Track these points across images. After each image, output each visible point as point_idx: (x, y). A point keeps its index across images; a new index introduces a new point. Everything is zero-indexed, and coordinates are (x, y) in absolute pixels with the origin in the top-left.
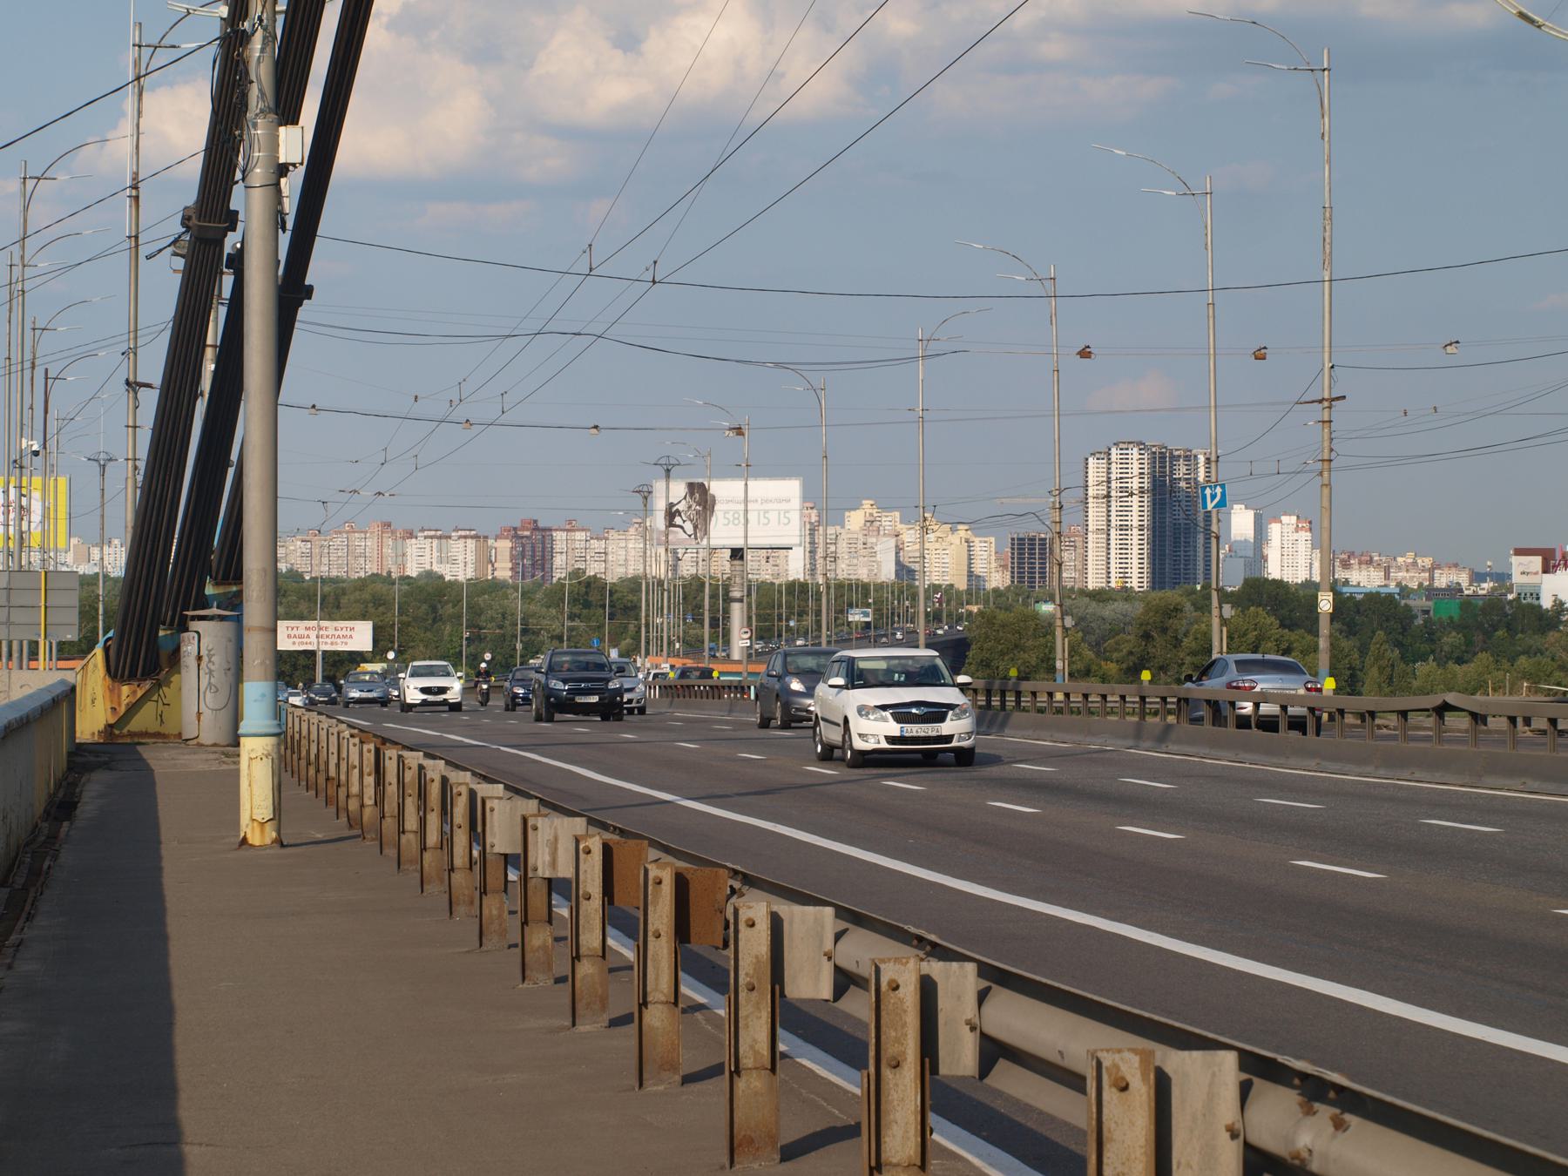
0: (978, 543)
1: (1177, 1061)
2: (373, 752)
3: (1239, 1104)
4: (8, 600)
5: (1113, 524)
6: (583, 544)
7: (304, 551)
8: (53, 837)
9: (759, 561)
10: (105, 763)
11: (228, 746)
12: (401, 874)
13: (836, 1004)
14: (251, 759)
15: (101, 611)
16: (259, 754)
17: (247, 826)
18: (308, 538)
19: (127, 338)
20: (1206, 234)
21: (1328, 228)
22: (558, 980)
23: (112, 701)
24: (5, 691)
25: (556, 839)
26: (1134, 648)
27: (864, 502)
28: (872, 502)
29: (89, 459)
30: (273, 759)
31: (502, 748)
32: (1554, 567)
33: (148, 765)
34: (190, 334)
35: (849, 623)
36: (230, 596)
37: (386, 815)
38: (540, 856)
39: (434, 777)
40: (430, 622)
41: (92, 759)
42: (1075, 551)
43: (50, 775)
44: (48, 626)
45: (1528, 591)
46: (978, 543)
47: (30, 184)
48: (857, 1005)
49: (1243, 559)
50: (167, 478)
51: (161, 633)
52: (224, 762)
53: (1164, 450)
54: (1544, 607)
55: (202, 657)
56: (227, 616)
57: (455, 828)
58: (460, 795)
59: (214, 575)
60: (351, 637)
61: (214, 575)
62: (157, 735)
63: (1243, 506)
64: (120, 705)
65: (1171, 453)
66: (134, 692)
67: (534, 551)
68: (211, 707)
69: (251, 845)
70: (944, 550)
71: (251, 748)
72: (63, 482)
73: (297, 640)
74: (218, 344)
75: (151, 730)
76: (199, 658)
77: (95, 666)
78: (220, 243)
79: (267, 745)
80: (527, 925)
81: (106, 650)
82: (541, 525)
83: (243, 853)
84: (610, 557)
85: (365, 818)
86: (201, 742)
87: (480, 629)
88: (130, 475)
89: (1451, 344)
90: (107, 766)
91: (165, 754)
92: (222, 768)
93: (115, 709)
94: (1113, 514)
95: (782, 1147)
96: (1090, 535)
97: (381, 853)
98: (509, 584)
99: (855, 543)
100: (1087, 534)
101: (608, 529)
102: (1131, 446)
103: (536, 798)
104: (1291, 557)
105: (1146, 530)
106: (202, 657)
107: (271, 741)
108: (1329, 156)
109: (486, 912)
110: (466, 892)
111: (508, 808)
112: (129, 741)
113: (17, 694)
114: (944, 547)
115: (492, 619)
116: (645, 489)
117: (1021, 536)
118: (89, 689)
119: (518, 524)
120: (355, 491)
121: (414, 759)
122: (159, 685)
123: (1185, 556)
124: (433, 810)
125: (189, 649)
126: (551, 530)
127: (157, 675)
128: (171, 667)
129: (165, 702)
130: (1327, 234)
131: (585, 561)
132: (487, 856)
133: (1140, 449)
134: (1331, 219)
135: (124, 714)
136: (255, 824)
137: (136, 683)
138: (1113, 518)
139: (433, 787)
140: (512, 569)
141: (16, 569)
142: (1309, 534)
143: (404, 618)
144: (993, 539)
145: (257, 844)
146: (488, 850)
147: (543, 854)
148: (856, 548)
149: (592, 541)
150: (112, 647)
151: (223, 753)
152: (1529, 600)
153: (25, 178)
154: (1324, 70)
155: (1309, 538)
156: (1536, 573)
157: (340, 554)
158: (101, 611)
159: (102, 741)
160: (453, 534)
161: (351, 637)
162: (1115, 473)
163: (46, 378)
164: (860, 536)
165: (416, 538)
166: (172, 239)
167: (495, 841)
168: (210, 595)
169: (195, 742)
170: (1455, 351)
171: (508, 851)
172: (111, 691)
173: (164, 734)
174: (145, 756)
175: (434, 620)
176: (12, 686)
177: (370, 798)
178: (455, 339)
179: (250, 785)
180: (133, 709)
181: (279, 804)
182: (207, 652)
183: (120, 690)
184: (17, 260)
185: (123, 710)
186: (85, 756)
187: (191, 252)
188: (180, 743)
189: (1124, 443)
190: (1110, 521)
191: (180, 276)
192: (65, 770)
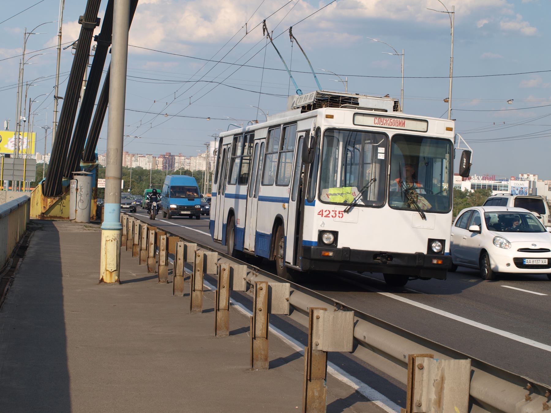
1: (188, 244)
2: (154, 234)
3: (470, 379)
4: (14, 168)
6: (183, 160)
8: (14, 267)
10: (41, 228)
11: (86, 223)
12: (192, 313)
13: (290, 317)
14: (107, 240)
15: (44, 174)
16: (111, 238)
17: (104, 273)
19: (56, 77)
20: (402, 68)
21: (452, 64)
22: (185, 295)
23: (44, 204)
24: (4, 199)
25: (443, 379)
29: (42, 128)
30: (117, 241)
31: (186, 227)
32: (465, 179)
33: (57, 229)
34: (75, 83)
36: (89, 167)
37: (177, 275)
38: (424, 393)
39: (225, 268)
40: (139, 181)
41: (36, 226)
43: (17, 235)
44: (26, 177)
45: (458, 186)
47: (27, 35)
48: (251, 294)
50: (68, 121)
51: (63, 180)
52: (85, 230)
54: (462, 191)
55: (78, 189)
56: (88, 174)
57: (257, 311)
58: (262, 289)
59: (83, 158)
61: (44, 194)
62: (60, 217)
64: (47, 206)
66: (52, 201)
67: (169, 162)
68: (81, 208)
69: (105, 282)
71: (106, 236)
72: (34, 134)
73: (101, 185)
74: (87, 80)
75: (58, 216)
76: (77, 189)
77: (38, 191)
78: (92, 31)
79: (115, 234)
80: (255, 339)
81: (43, 185)
82: (172, 154)
83: (101, 287)
84: (191, 165)
85: (161, 271)
86: (76, 221)
87: (154, 183)
88: (54, 127)
89: (510, 100)
90: (41, 229)
91: (63, 225)
92: (84, 232)
93: (45, 207)
95: (230, 332)
97: (174, 294)
98: (161, 171)
101: (191, 157)
103: (147, 223)
106: (78, 189)
107: (117, 232)
108: (453, 41)
109: (310, 393)
110: (263, 353)
111: (331, 317)
112: (49, 219)
113: (8, 200)
115: (157, 181)
116: (208, 144)
118: (36, 199)
119: (165, 154)
120: (128, 136)
121: (192, 247)
122: (61, 199)
124: (224, 287)
125: (73, 186)
126: (174, 156)
127: (61, 195)
128: (66, 193)
129: (63, 205)
130: (451, 66)
132: (313, 352)
134: (453, 62)
135: (48, 209)
136: (108, 272)
137: (53, 198)
139: (261, 293)
140: (163, 167)
141: (17, 158)
143: (133, 180)
145: (108, 282)
146: (313, 348)
147: (428, 393)
149: (186, 160)
150: (45, 184)
151: (85, 226)
152: (458, 189)
153: (25, 33)
154: (452, 13)
156: (460, 181)
158: (44, 174)
159: (40, 219)
160: (146, 156)
163: (30, 101)
166: (73, 43)
167: (320, 342)
168: (81, 166)
169: (74, 221)
170: (511, 103)
171: (330, 350)
172: (44, 200)
173: (63, 217)
174: (56, 225)
175: (140, 180)
176: (7, 197)
177: (163, 262)
178: (168, 82)
179: (106, 253)
180: (52, 207)
181: (120, 263)
182: (80, 187)
183: (47, 200)
184: (22, 62)
185: (48, 207)
186: (33, 225)
187: (78, 47)
188: (68, 221)
191: (74, 56)
192: (25, 230)
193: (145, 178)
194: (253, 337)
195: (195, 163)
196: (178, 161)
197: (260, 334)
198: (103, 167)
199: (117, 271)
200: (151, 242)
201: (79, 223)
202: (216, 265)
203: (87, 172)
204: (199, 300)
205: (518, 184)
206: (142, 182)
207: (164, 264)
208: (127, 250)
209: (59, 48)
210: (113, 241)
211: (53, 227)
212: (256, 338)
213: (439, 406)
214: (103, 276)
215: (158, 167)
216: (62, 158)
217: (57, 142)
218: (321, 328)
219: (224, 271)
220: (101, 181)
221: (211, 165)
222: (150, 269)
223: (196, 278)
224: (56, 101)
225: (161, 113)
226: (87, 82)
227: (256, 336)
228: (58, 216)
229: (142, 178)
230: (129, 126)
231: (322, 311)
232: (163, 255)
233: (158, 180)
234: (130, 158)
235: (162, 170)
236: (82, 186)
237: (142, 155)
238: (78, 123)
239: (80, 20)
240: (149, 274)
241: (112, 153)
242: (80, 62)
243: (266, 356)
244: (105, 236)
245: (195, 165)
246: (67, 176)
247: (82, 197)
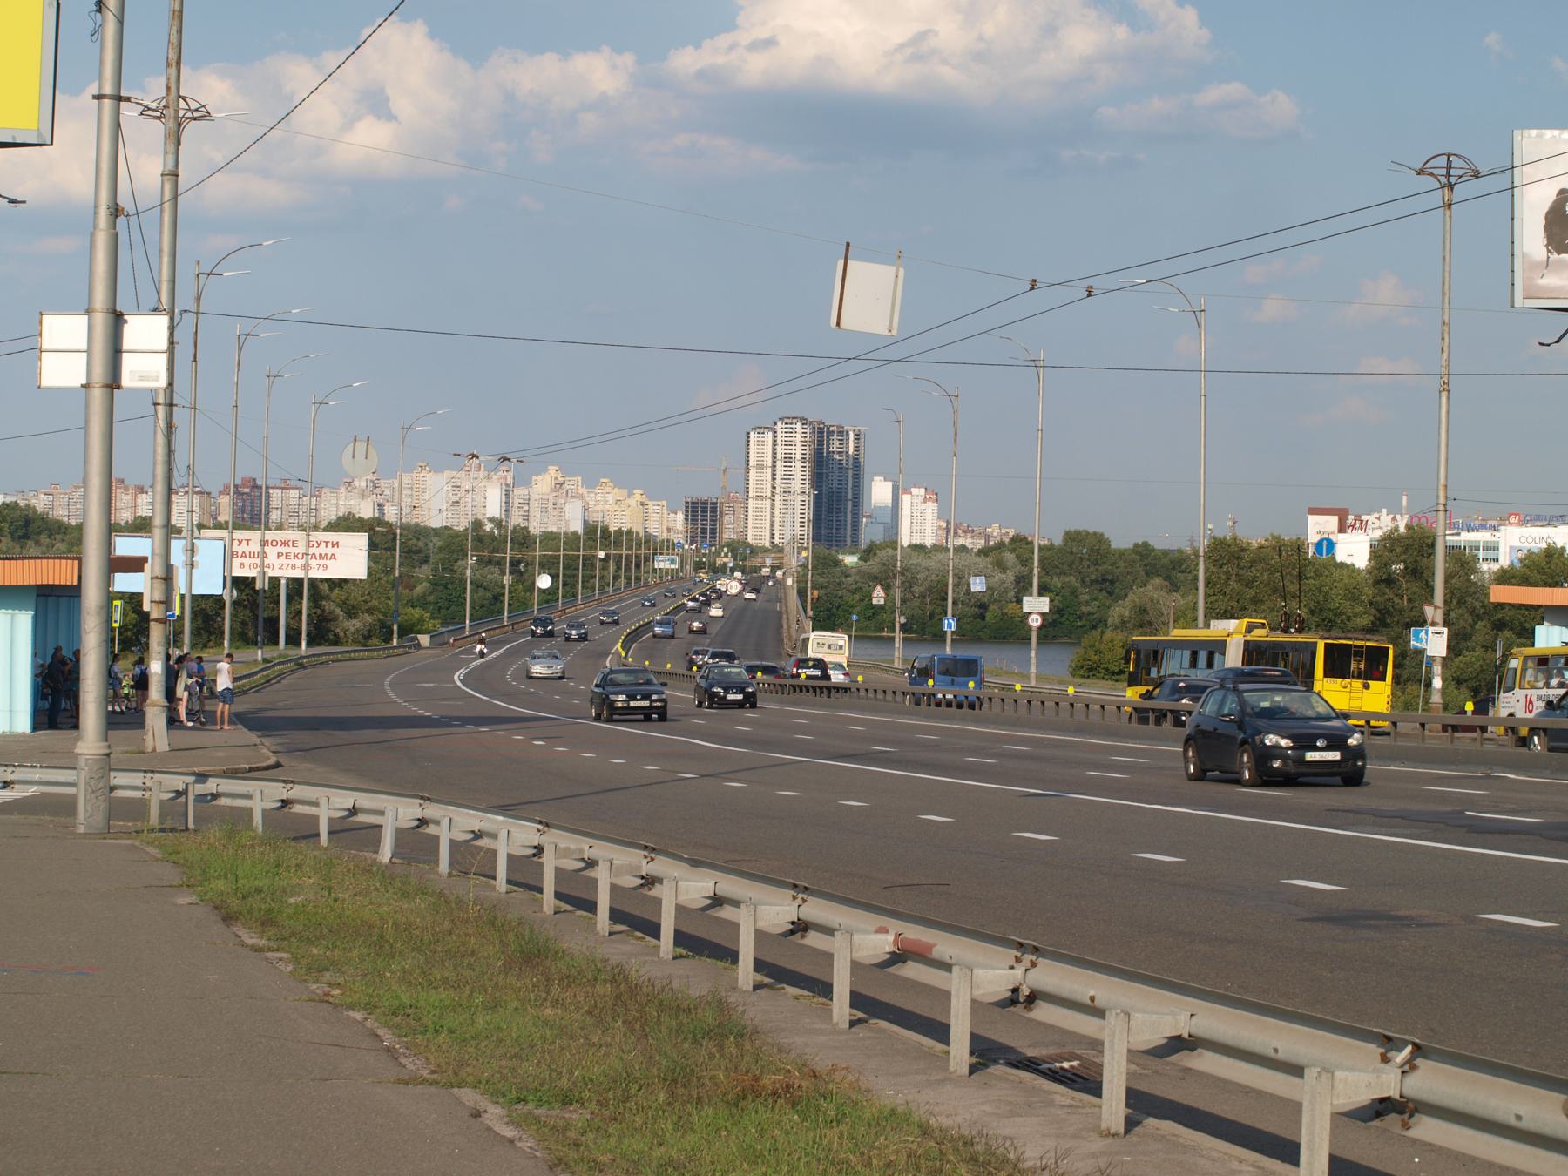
0: (652, 506)
7: (47, 503)
9: (459, 518)
18: (50, 492)
26: (1373, 597)
27: (550, 467)
28: (557, 468)
35: (654, 570)
42: (734, 514)
46: (652, 506)
49: (883, 525)
53: (822, 426)
60: (333, 557)
63: (882, 478)
65: (828, 429)
96: (750, 501)
99: (546, 504)
102: (795, 421)
104: (919, 524)
114: (623, 509)
117: (694, 500)
123: (837, 521)
131: (298, 516)
133: (803, 424)
142: (935, 504)
144: (665, 503)
155: (936, 508)
157: (78, 507)
161: (333, 557)
165: (147, 493)
189: (789, 418)
205: (1534, 540)
220: (248, 541)
221: (384, 514)
234: (129, 497)
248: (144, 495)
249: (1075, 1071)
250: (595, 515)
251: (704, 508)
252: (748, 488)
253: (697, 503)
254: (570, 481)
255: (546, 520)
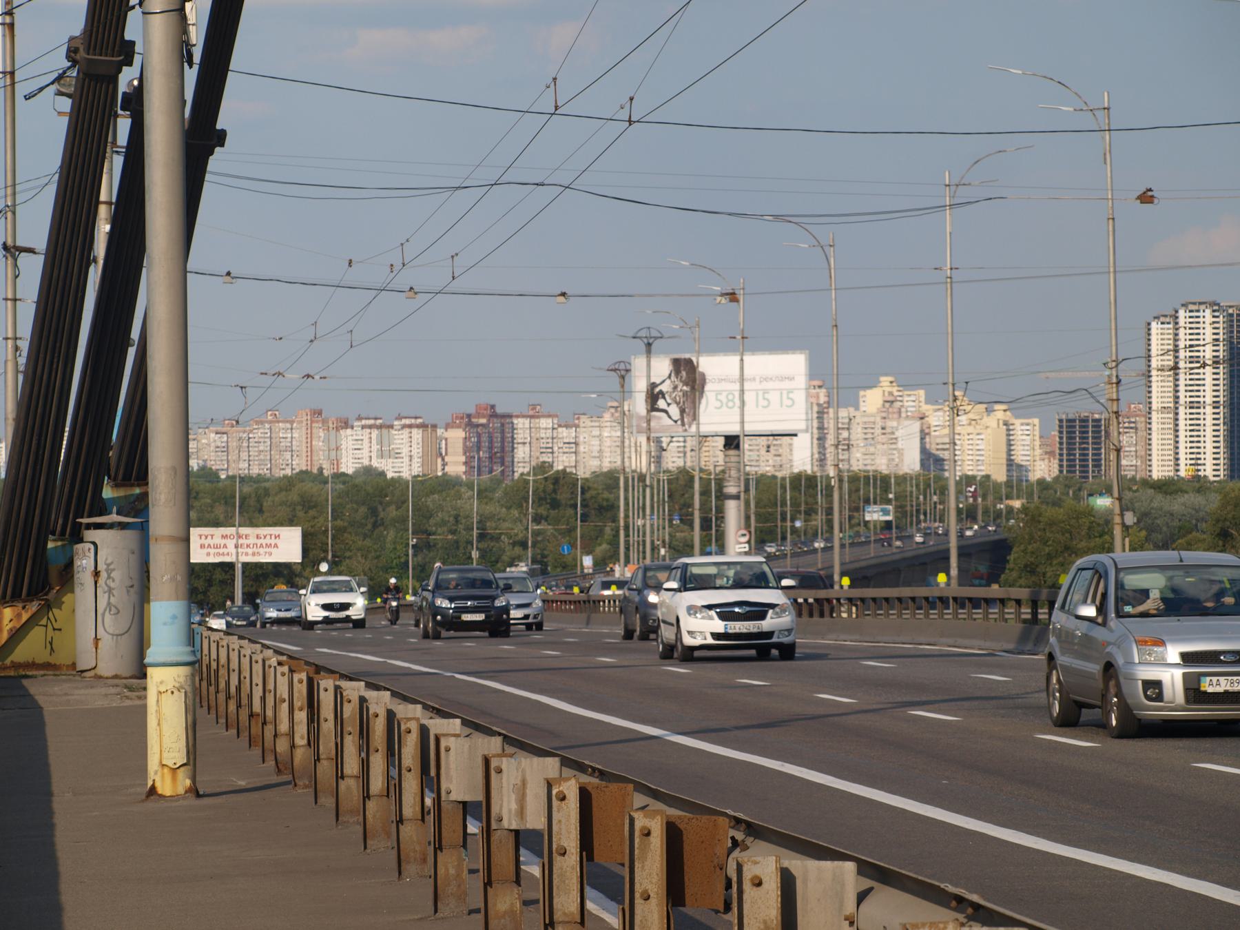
2: (305, 682)
5: (1182, 400)
7: (219, 444)
9: (758, 450)
11: (131, 677)
12: (340, 827)
16: (170, 687)
17: (156, 773)
18: (224, 430)
25: (524, 783)
27: (882, 379)
30: (186, 693)
34: (71, 244)
36: (132, 499)
38: (505, 804)
40: (369, 526)
42: (1136, 433)
50: (56, 360)
51: (50, 545)
52: (127, 697)
56: (128, 523)
57: (404, 771)
59: (113, 474)
60: (276, 546)
62: (47, 666)
66: (19, 616)
68: (111, 632)
70: (978, 434)
71: (159, 681)
73: (212, 551)
74: (114, 200)
76: (96, 574)
82: (499, 410)
83: (151, 805)
84: (581, 448)
86: (99, 674)
87: (430, 534)
92: (125, 704)
94: (1182, 388)
96: (1154, 415)
97: (316, 803)
98: (462, 479)
99: (873, 428)
100: (1150, 413)
101: (578, 415)
102: (1202, 307)
103: (500, 734)
105: (1222, 407)
107: (183, 671)
111: (467, 746)
112: (12, 673)
116: (622, 366)
117: (1071, 416)
119: (472, 410)
120: (279, 374)
122: (48, 606)
124: (377, 751)
125: (84, 562)
126: (511, 416)
127: (46, 594)
129: (56, 627)
133: (1214, 311)
135: (6, 642)
137: (20, 605)
138: (1182, 394)
139: (409, 739)
140: (465, 463)
143: (339, 523)
144: (1036, 421)
145: (168, 794)
147: (509, 802)
148: (873, 433)
149: (560, 430)
151: (126, 687)
157: (261, 448)
160: (396, 423)
161: (276, 546)
162: (1183, 340)
164: (878, 419)
165: (352, 427)
166: (55, 75)
171: (467, 799)
173: (55, 665)
174: (32, 691)
175: (375, 526)
177: (302, 738)
179: (159, 724)
180: (17, 635)
182: (105, 567)
188: (74, 675)
189: (1194, 303)
190: (1178, 397)
193: (392, 512)
194: (547, 922)
195: (596, 442)
196: (528, 436)
197: (411, 814)
198: (223, 477)
199: (188, 767)
200: (281, 695)
201: (107, 678)
202: (851, 924)
203: (125, 516)
204: (355, 798)
206: (381, 528)
207: (305, 742)
208: (238, 737)
209: (8, 69)
210: (176, 692)
211: (24, 696)
212: (405, 822)
213: (522, 818)
214: (154, 780)
215: (444, 465)
216: (38, 511)
217: (25, 427)
218: (452, 766)
219: (377, 719)
220: (212, 536)
222: (280, 766)
223: (344, 749)
224: (10, 261)
225: (390, 287)
226: (113, 206)
227: (404, 818)
228: (41, 662)
229: (382, 515)
230: (281, 339)
231: (453, 739)
232: (301, 721)
233: (447, 519)
235: (464, 477)
236: (112, 563)
237: (379, 422)
238: (87, 364)
239: (70, 51)
240: (280, 777)
241: (163, 480)
242: (86, 148)
243: (424, 854)
244: (155, 683)
245: (596, 448)
246: (63, 533)
247: (113, 596)
248: (349, 431)
249: (494, 826)
250: (939, 440)
251: (1084, 427)
252: (1150, 397)
253: (1074, 421)
254: (909, 395)
255: (872, 449)
